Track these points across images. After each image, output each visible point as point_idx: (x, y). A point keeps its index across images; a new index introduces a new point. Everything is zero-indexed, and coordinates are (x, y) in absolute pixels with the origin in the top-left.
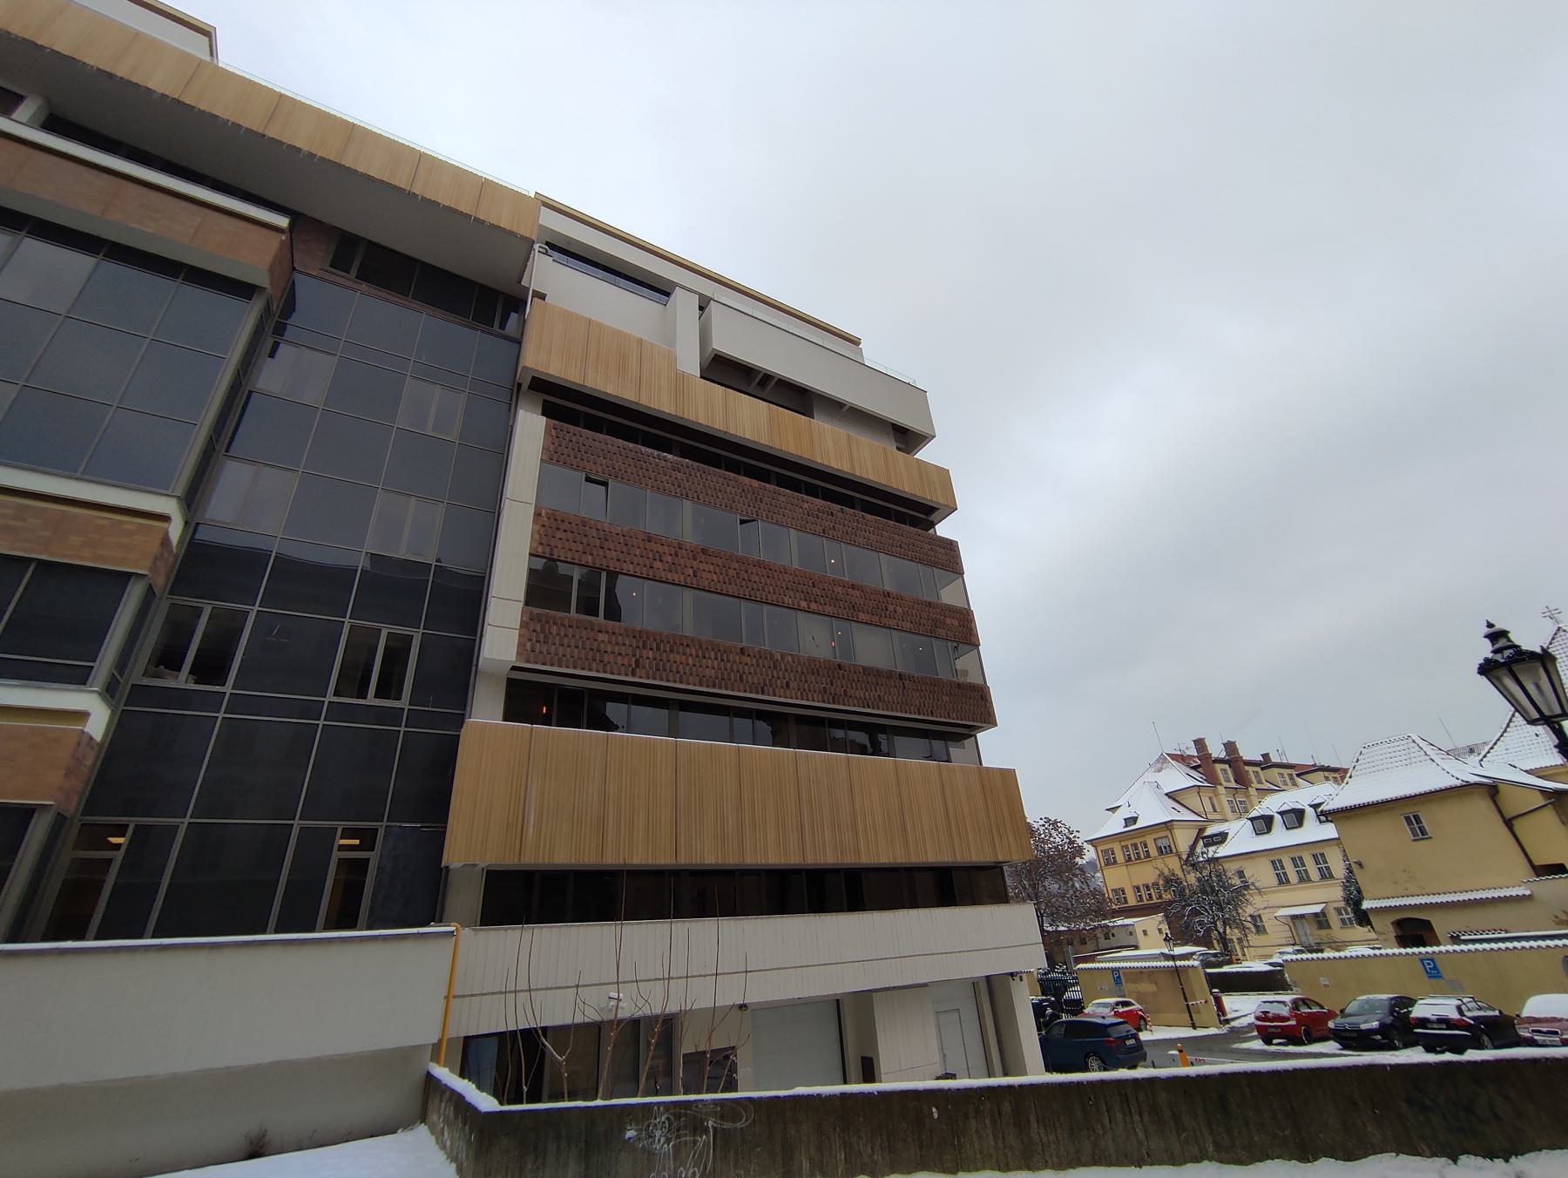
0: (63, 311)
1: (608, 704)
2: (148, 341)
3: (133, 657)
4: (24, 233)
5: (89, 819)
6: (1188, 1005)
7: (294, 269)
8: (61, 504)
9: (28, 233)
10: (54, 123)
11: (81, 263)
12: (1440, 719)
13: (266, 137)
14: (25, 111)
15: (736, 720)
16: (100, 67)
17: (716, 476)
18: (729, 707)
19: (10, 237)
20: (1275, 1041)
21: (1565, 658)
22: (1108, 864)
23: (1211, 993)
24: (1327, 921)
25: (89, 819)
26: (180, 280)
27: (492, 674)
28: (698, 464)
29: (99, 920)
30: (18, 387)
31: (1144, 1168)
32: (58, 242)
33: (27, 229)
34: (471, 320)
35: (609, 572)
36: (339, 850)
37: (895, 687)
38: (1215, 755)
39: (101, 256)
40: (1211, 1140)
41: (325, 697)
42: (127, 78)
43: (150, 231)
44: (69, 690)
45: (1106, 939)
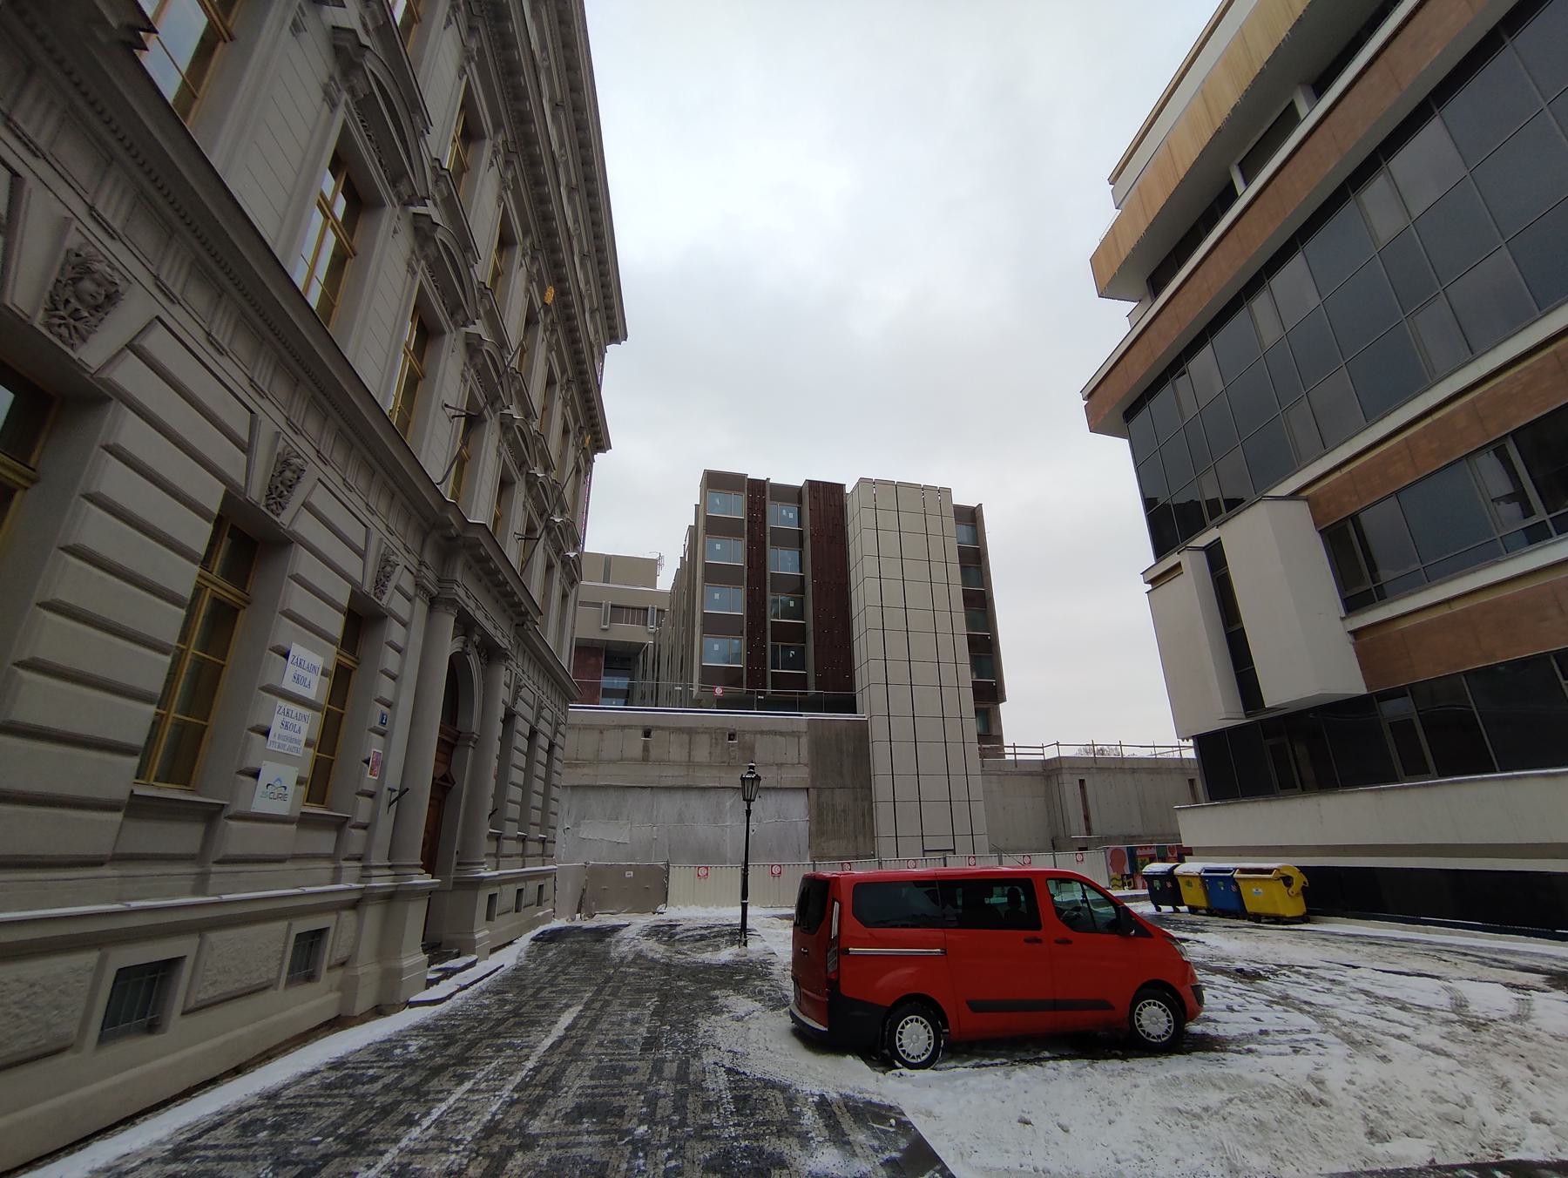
0: (1466, 172)
2: (1546, 110)
4: (1384, 164)
8: (1547, 347)
9: (1386, 160)
10: (1319, 87)
11: (1432, 134)
14: (1302, 108)
16: (1289, 28)
19: (1382, 176)
20: (1263, 921)
21: (551, 1174)
22: (643, 760)
26: (1508, 41)
30: (1504, 247)
32: (1309, 238)
33: (1350, 192)
38: (1053, 881)
39: (1437, 112)
41: (1544, 521)
42: (1305, 6)
43: (1438, 52)
44: (1537, 549)
45: (1083, 780)
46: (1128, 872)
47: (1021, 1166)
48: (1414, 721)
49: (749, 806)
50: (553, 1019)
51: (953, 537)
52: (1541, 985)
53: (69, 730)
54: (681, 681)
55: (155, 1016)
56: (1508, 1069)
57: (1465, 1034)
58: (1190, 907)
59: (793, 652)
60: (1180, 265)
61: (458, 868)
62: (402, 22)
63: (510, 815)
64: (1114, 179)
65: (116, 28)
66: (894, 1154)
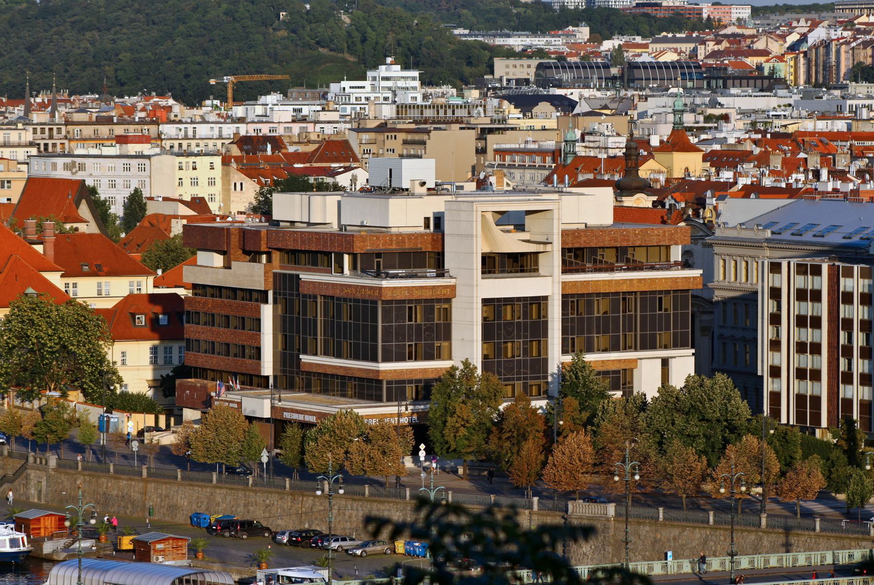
1: (434, 160)
3: (166, 481)
5: (230, 95)
6: (211, 468)
7: (733, 130)
12: (391, 170)
13: (485, 315)
15: (100, 153)
17: (711, 342)
18: (779, 405)
23: (216, 463)
24: (397, 382)
25: (230, 95)
27: (258, 386)
28: (643, 227)
29: (272, 283)
31: (773, 4)
34: (359, 272)
35: (335, 253)
36: (53, 144)
37: (357, 510)
38: (278, 253)
40: (621, 43)
45: (101, 283)
46: (571, 126)
47: (166, 230)
48: (375, 513)
49: (787, 539)
50: (268, 84)
51: (447, 203)
52: (535, 186)
53: (378, 200)
54: (519, 373)
55: (799, 511)
56: (111, 365)
57: (639, 55)
58: (515, 226)
59: (284, 13)
60: (829, 412)
61: (442, 310)
62: (41, 275)
63: (332, 219)
64: (420, 157)
65: (301, 356)
66: (117, 100)
